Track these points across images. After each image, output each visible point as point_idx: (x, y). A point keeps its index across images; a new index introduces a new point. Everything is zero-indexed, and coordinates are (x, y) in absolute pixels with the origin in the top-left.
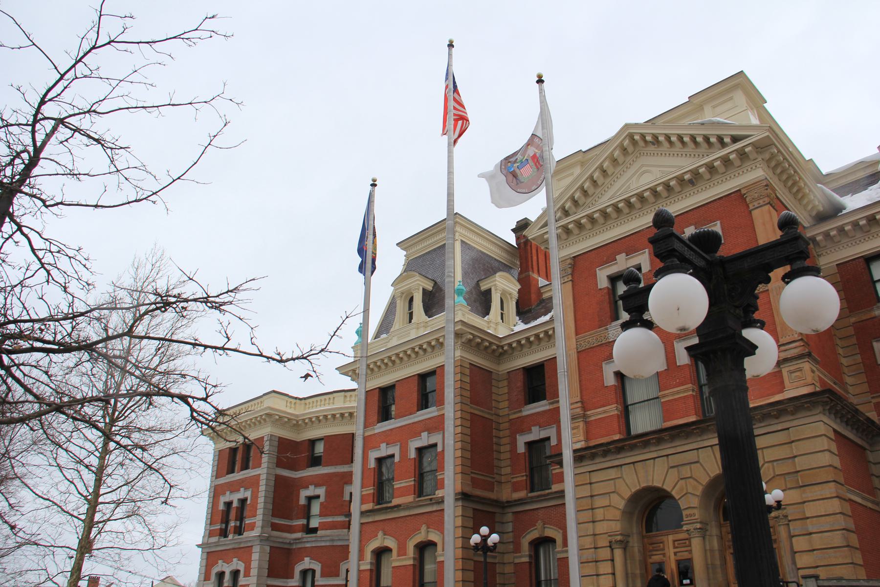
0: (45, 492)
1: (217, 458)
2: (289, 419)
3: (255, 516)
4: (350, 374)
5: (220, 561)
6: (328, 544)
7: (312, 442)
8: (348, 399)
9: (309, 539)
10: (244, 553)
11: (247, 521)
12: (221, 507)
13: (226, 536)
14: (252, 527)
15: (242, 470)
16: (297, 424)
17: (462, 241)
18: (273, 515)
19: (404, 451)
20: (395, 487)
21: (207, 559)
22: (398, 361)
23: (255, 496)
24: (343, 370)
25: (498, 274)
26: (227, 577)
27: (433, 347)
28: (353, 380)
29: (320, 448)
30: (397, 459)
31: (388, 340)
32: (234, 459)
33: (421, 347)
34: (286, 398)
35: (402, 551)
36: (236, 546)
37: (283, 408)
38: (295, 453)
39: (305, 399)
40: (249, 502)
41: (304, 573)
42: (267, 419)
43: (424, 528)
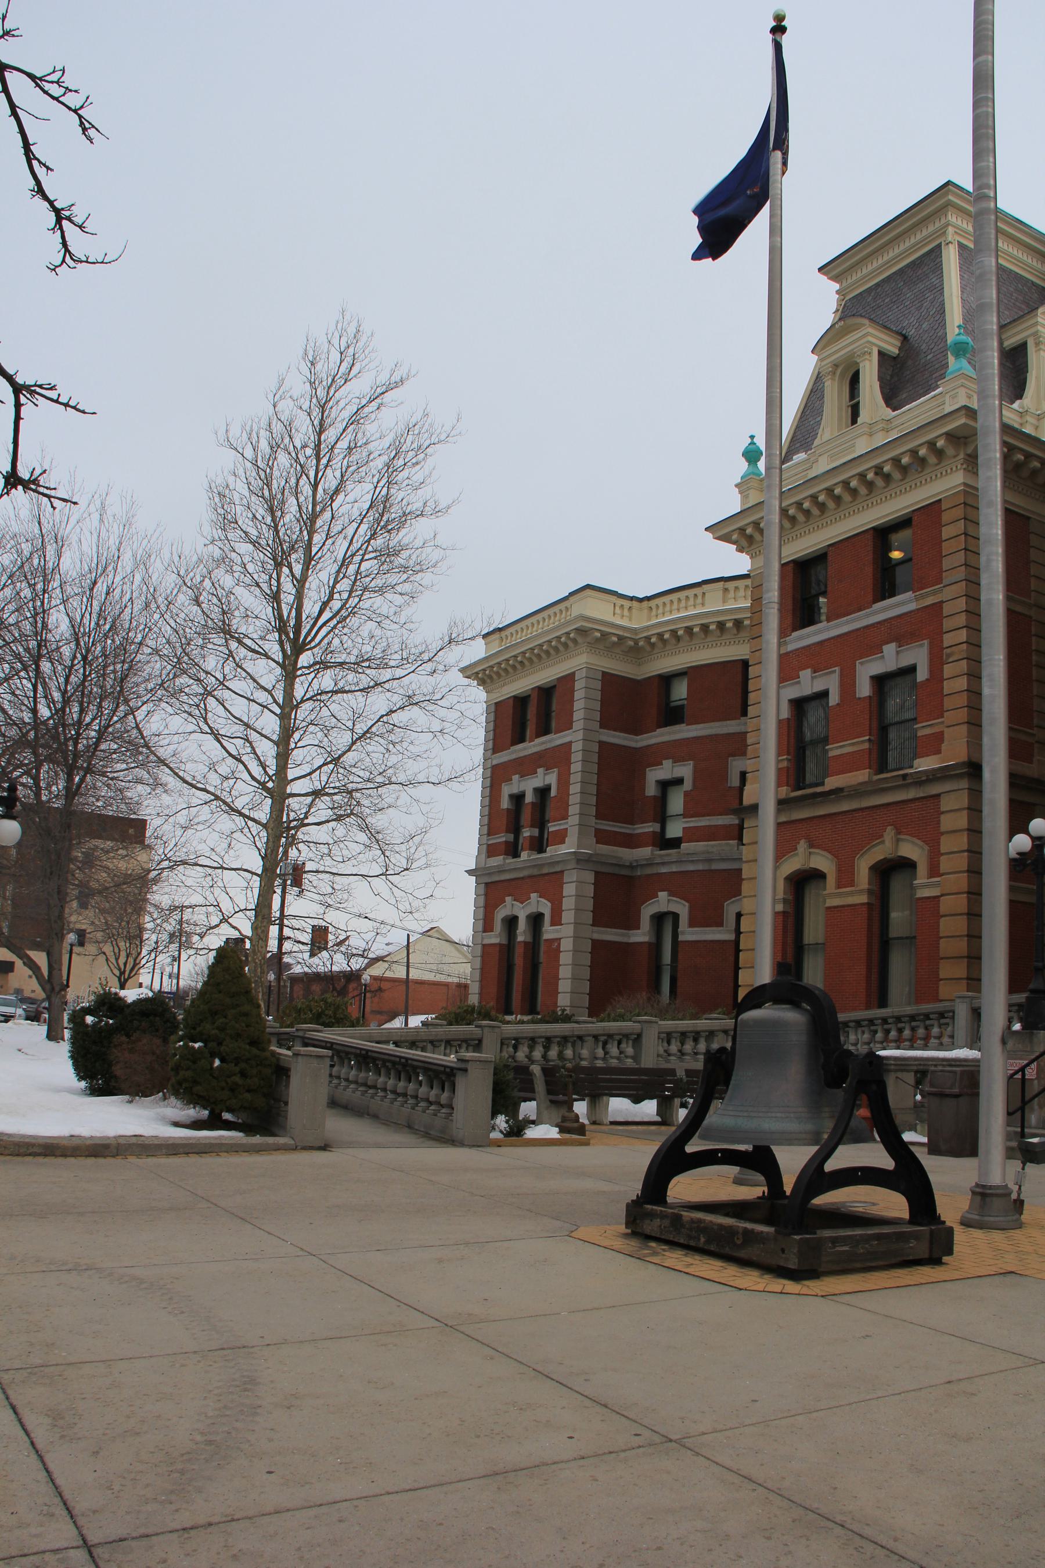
0: (198, 778)
1: (492, 717)
2: (621, 638)
3: (565, 817)
4: (735, 537)
5: (508, 899)
6: (700, 867)
7: (666, 680)
8: (732, 594)
9: (666, 859)
10: (549, 883)
11: (553, 827)
12: (505, 804)
13: (516, 855)
14: (561, 837)
15: (538, 736)
16: (635, 646)
17: (961, 246)
18: (604, 724)
19: (848, 684)
20: (831, 754)
21: (486, 895)
22: (831, 504)
23: (564, 782)
24: (721, 531)
25: (1040, 310)
26: (522, 925)
27: (904, 470)
28: (740, 550)
29: (680, 691)
30: (834, 699)
31: (809, 464)
32: (521, 719)
33: (878, 470)
34: (613, 599)
35: (846, 877)
36: (535, 872)
37: (608, 617)
38: (637, 701)
39: (648, 599)
40: (553, 793)
41: (659, 919)
42: (580, 640)
43: (889, 833)
